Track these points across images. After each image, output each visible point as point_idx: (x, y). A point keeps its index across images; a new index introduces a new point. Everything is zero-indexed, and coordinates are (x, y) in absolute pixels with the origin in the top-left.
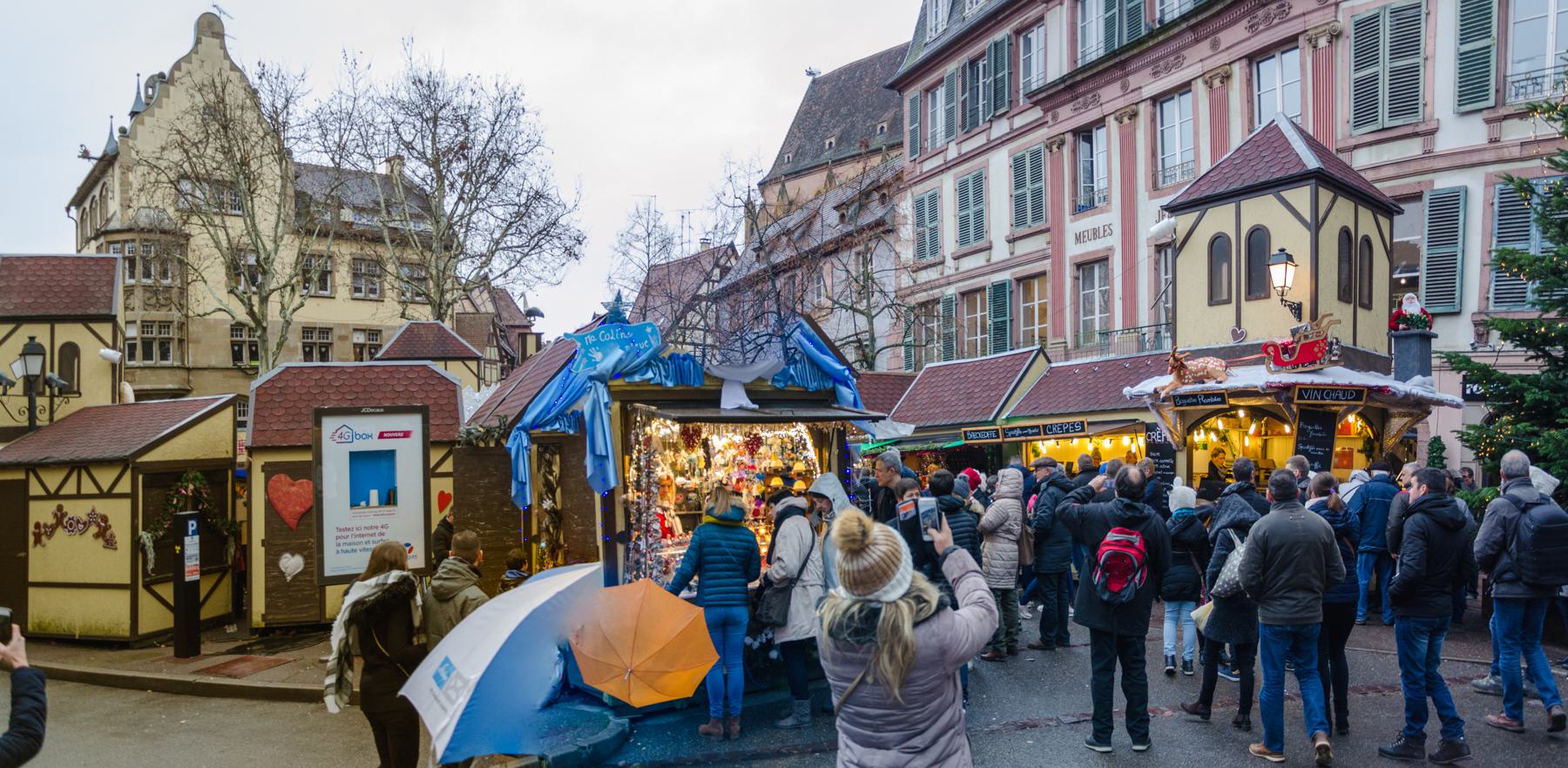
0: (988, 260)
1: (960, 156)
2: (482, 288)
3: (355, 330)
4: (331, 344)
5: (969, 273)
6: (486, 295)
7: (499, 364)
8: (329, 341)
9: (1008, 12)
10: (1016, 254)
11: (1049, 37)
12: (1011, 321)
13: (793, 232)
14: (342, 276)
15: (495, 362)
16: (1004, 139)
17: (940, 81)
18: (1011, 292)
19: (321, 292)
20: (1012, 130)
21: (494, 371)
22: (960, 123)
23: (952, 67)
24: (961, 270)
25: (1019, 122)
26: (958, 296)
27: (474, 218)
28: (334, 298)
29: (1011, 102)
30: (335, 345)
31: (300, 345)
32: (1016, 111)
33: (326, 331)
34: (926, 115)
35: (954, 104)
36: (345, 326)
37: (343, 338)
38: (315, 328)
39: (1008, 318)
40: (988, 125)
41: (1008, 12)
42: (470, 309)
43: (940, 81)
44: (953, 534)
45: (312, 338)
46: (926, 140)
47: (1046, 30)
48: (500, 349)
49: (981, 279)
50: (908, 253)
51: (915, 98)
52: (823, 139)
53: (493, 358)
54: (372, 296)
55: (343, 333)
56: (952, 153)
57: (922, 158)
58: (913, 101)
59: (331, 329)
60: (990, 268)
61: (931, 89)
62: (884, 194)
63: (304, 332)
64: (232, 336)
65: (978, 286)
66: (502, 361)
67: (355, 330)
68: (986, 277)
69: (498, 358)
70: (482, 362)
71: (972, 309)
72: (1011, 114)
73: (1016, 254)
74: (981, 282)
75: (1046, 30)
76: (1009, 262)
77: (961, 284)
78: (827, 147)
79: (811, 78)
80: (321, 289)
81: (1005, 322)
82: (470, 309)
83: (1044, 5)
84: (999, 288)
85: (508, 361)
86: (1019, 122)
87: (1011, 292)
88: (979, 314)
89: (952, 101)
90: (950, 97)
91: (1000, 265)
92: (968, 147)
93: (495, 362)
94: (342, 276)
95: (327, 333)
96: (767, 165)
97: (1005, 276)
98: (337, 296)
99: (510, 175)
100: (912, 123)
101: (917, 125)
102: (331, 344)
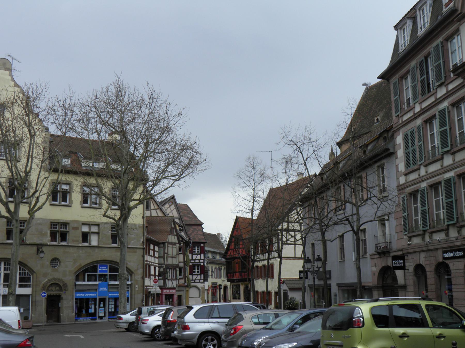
0: (442, 166)
1: (422, 109)
2: (171, 203)
3: (83, 224)
4: (68, 232)
5: (433, 174)
6: (173, 207)
7: (178, 245)
8: (67, 230)
9: (439, 29)
10: (456, 160)
11: (462, 39)
12: (456, 201)
13: (339, 163)
14: (76, 197)
15: (175, 244)
16: (444, 97)
17: (408, 72)
18: (455, 184)
19: (63, 203)
20: (448, 92)
21: (174, 249)
22: (420, 92)
23: (413, 63)
24: (429, 172)
25: (451, 87)
26: (428, 188)
27: (23, 130)
28: (70, 206)
29: (445, 77)
30: (70, 232)
31: (49, 232)
32: (449, 81)
33: (65, 224)
34: (403, 90)
35: (416, 82)
36: (77, 222)
37: (76, 229)
38: (58, 223)
39: (453, 199)
40: (435, 91)
41: (439, 29)
42: (160, 214)
43: (408, 72)
44: (301, 309)
45: (56, 228)
46: (404, 104)
47: (461, 36)
48: (179, 236)
49: (439, 177)
50: (402, 167)
51: (396, 82)
52: (373, 117)
53: (174, 241)
54: (94, 206)
55: (76, 225)
56: (417, 109)
57: (402, 114)
58: (395, 84)
59: (68, 223)
60: (442, 170)
61: (404, 77)
62: (385, 137)
63: (51, 225)
64: (8, 225)
65: (438, 181)
66: (179, 243)
67: (83, 224)
68: (442, 176)
69: (177, 241)
70: (166, 244)
71: (437, 195)
72: (446, 83)
73: (456, 160)
74: (439, 178)
75: (461, 36)
76: (453, 166)
77: (429, 181)
78: (376, 121)
79: (365, 87)
80: (63, 201)
81: (452, 202)
82: (160, 214)
83: (459, 23)
84: (448, 181)
85: (184, 243)
86: (451, 87)
87: (455, 184)
88: (441, 197)
89: (415, 81)
90: (413, 80)
91: (448, 168)
92: (425, 105)
93: (175, 244)
94: (76, 197)
95: (66, 226)
96: (342, 134)
97: (450, 174)
98: (72, 205)
99: (166, 138)
100: (395, 96)
101: (398, 96)
102: (68, 232)
